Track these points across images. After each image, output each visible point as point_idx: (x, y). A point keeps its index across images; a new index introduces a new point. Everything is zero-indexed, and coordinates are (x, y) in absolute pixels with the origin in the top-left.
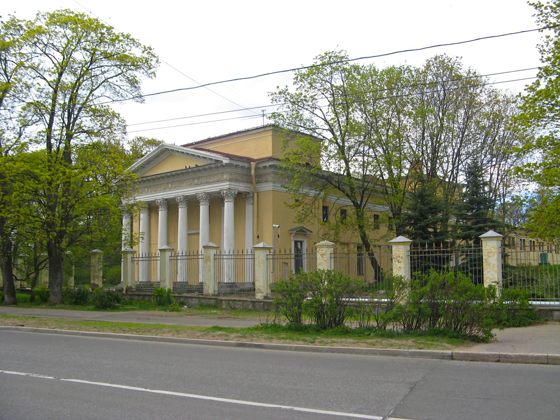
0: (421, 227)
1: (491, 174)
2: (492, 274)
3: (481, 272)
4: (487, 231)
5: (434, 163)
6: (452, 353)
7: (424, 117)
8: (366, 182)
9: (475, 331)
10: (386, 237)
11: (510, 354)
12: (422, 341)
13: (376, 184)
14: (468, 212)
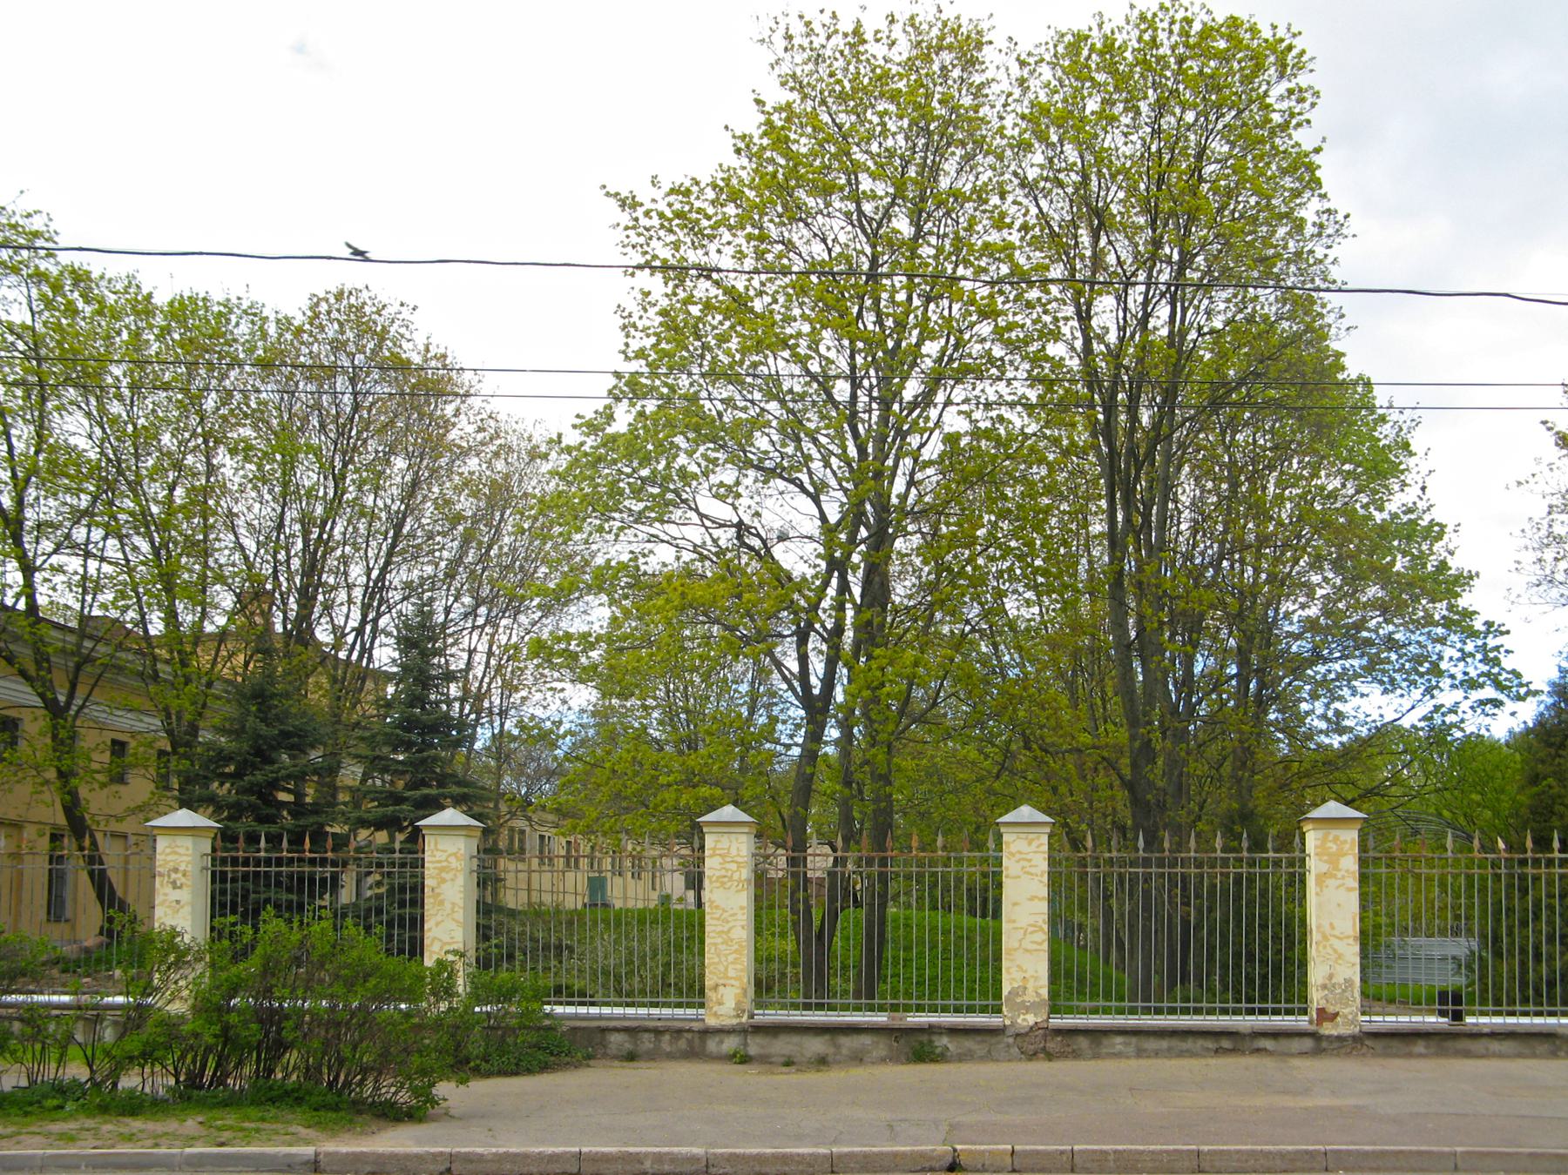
0: (252, 784)
1: (468, 651)
2: (448, 927)
3: (417, 923)
4: (443, 808)
5: (306, 600)
6: (317, 1154)
7: (289, 466)
8: (91, 637)
9: (391, 1090)
10: (145, 810)
11: (479, 1150)
12: (229, 1122)
13: (120, 647)
14: (395, 751)
